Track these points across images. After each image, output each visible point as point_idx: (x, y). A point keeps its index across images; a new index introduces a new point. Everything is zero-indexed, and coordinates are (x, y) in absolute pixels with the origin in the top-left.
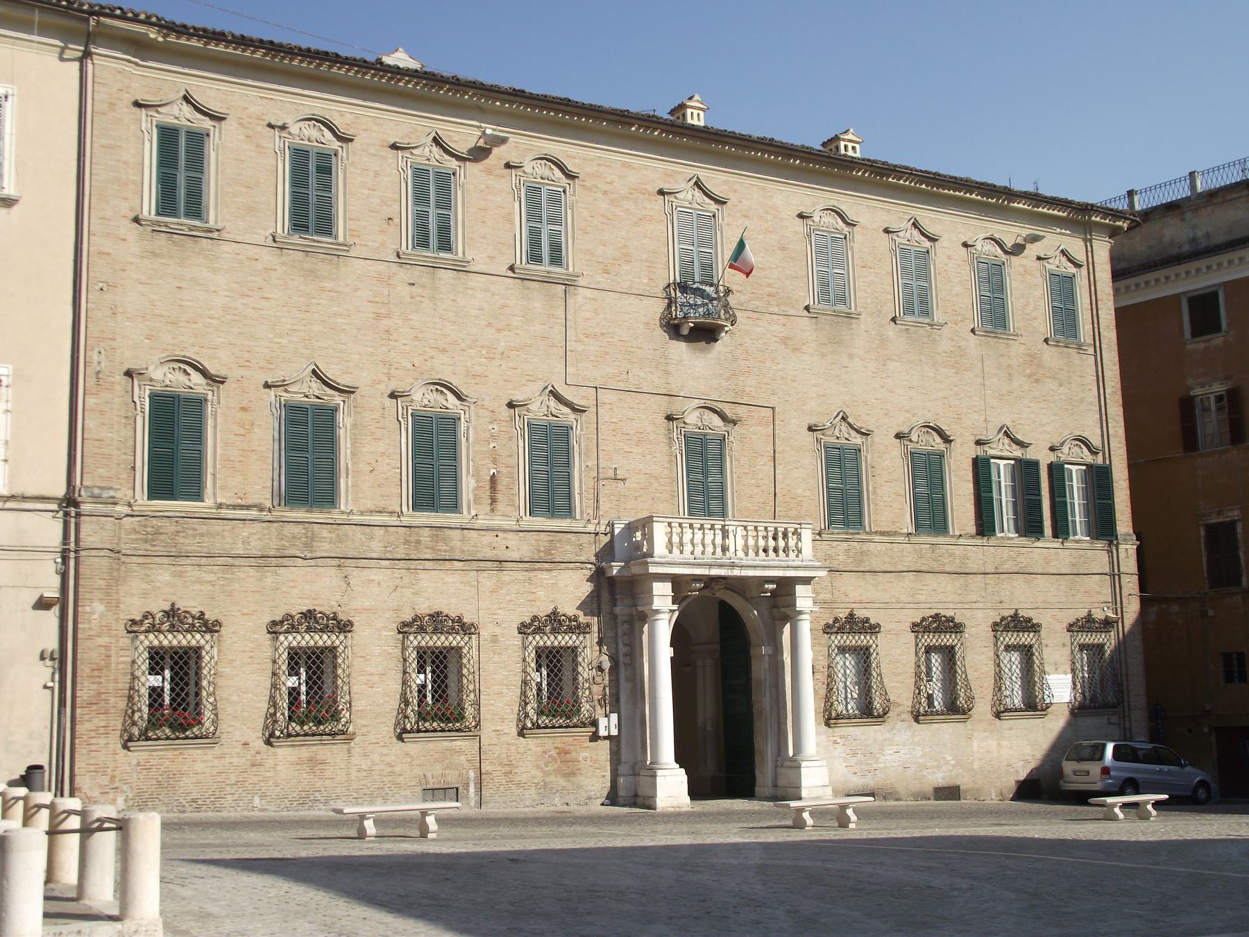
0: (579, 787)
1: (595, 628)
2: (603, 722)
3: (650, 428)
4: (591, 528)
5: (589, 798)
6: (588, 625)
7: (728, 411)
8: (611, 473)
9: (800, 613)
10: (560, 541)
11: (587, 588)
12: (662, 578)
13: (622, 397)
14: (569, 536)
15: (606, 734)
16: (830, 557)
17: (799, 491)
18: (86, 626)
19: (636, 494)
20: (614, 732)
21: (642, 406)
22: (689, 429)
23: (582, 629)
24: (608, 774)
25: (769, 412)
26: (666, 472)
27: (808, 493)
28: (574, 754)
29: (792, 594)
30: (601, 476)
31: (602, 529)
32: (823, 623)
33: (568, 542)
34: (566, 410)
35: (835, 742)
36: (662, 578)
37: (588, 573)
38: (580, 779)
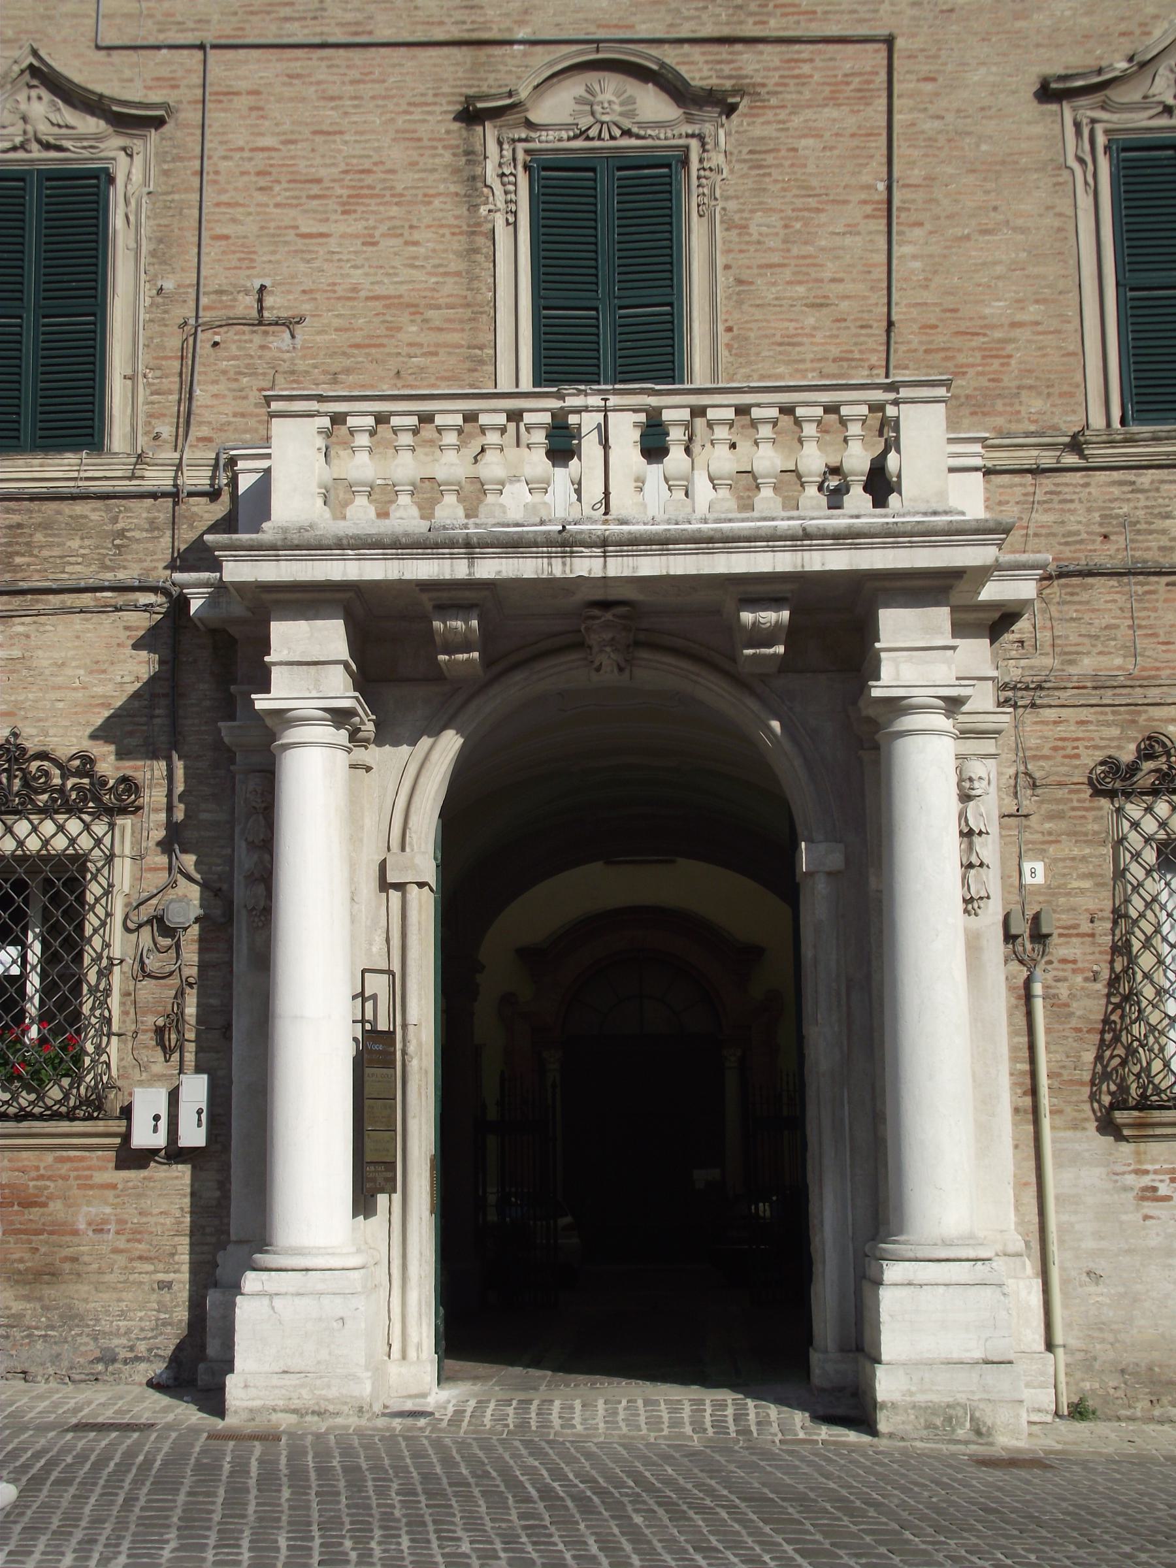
0: (71, 1317)
1: (154, 796)
2: (148, 1103)
3: (396, 155)
4: (158, 478)
5: (108, 1358)
6: (129, 784)
7: (698, 69)
8: (246, 305)
9: (896, 706)
10: (46, 526)
11: (137, 668)
12: (308, 600)
13: (296, 67)
14: (80, 508)
15: (159, 1140)
16: (1127, 523)
17: (995, 309)
18: (1019, 1066)
19: (337, 364)
20: (193, 1135)
21: (368, 90)
22: (547, 140)
23: (119, 801)
24: (182, 1277)
25: (875, 56)
26: (451, 288)
27: (1033, 311)
28: (56, 1206)
29: (867, 631)
30: (205, 316)
31: (197, 478)
32: (1090, 759)
33: (78, 526)
34: (91, 124)
35: (1149, 1194)
36: (308, 600)
37: (141, 622)
38: (82, 1295)
